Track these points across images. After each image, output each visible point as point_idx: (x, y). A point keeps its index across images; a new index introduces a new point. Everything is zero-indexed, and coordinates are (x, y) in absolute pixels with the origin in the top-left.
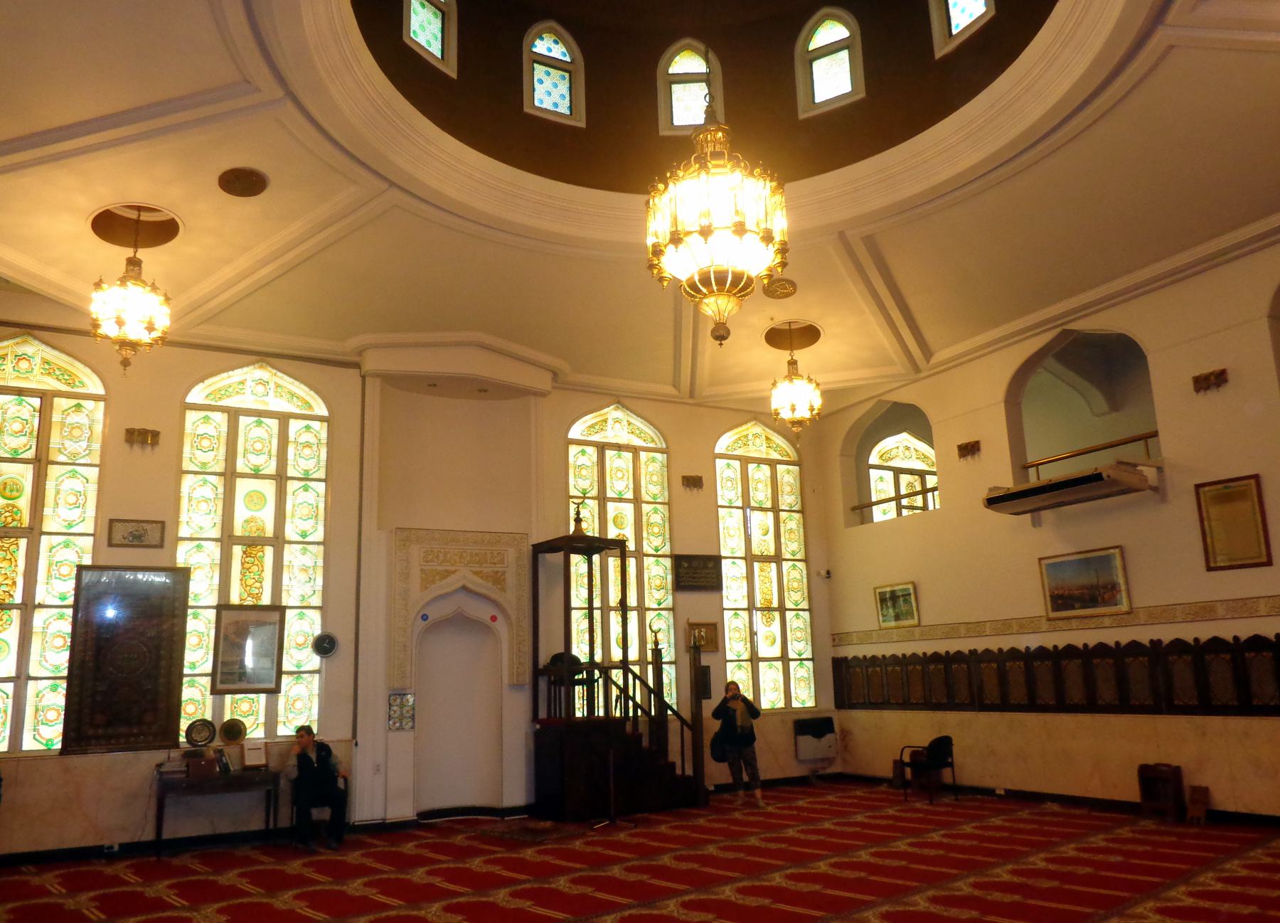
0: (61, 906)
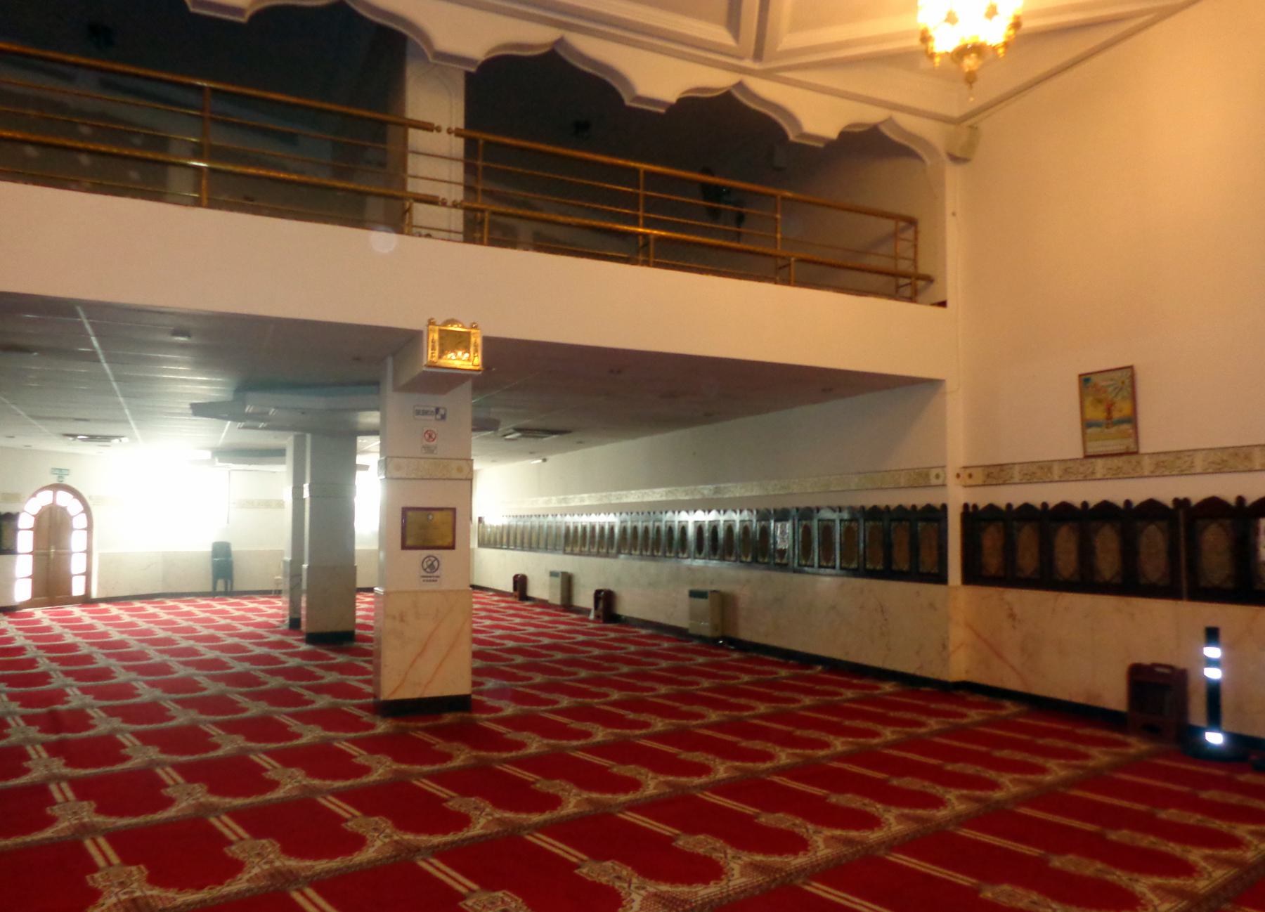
0: (163, 751)
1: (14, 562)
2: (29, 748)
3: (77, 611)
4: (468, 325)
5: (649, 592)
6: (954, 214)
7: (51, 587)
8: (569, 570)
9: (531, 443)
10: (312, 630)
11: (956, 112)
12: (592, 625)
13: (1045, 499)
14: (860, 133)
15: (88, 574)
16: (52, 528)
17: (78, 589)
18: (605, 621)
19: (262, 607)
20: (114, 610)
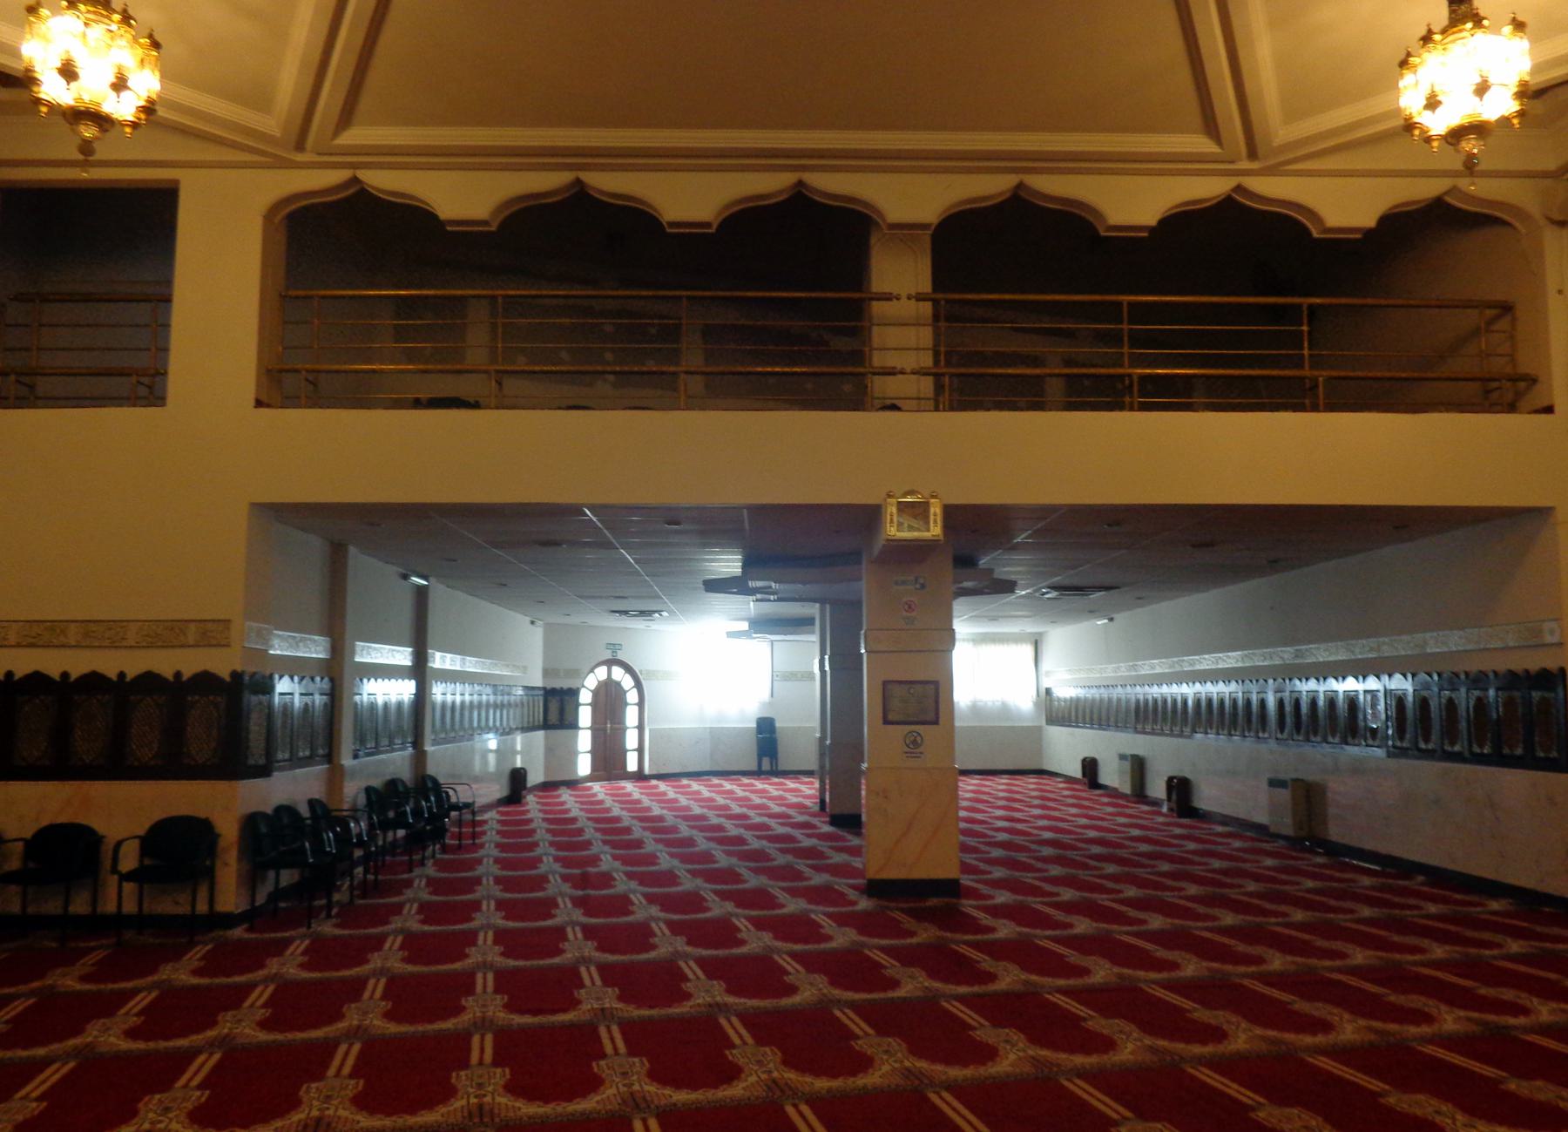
1: (576, 736)
2: (560, 900)
3: (629, 786)
4: (926, 494)
5: (1233, 781)
6: (1560, 292)
7: (608, 760)
8: (1140, 752)
9: (1077, 601)
10: (837, 811)
11: (1551, 164)
12: (1161, 819)
13: (1526, 666)
14: (1417, 211)
15: (640, 750)
16: (609, 702)
17: (632, 765)
18: (1180, 816)
19: (802, 787)
20: (662, 786)
